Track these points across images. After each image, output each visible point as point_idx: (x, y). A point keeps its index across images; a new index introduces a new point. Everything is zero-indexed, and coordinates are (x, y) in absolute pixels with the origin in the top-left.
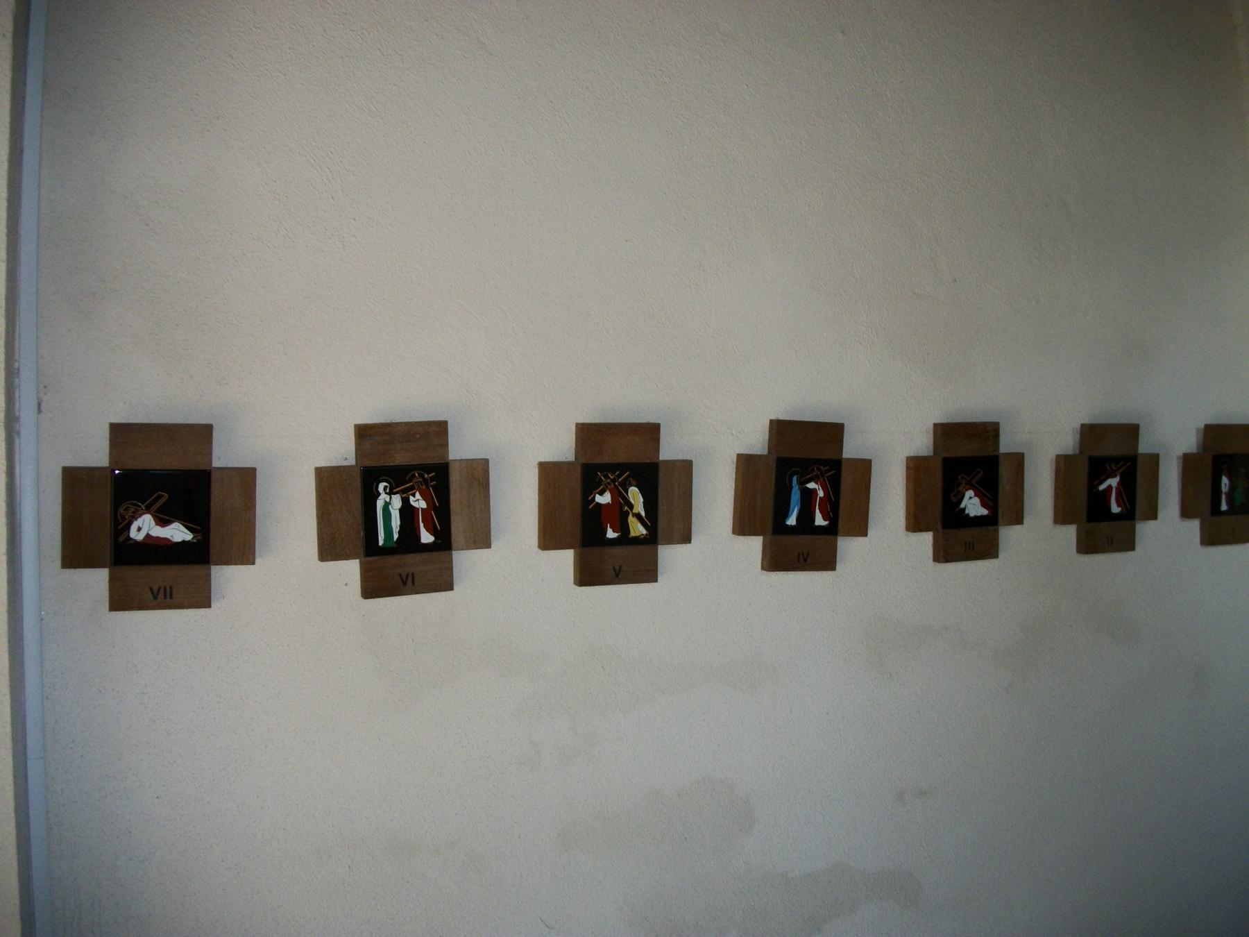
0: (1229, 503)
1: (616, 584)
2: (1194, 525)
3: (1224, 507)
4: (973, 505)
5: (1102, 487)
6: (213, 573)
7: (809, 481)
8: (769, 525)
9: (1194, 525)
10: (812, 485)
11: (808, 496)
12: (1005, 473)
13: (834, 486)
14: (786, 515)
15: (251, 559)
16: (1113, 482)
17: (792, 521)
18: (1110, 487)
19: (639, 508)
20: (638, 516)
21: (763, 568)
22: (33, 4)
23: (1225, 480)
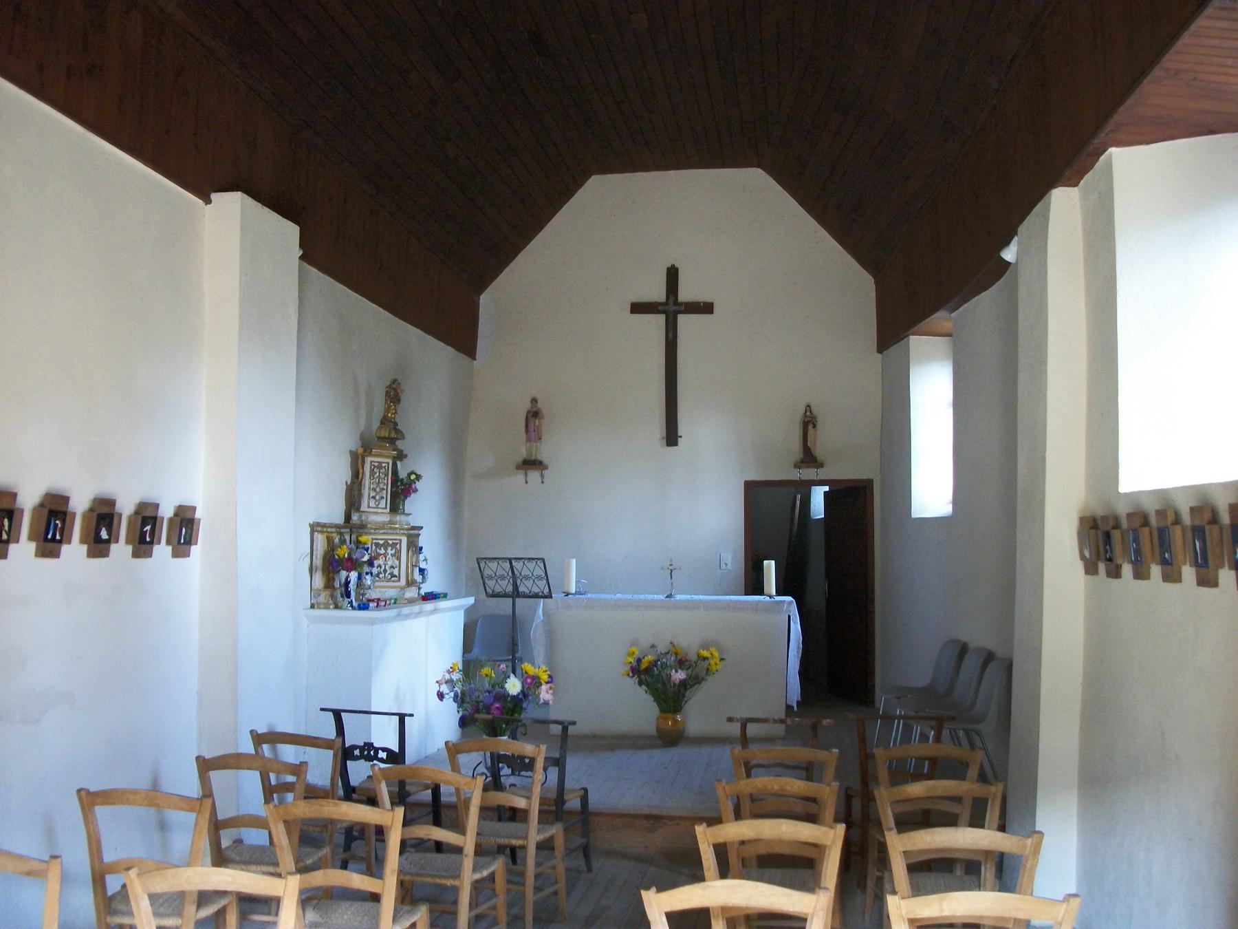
0: (185, 539)
1: (1039, 707)
2: (85, 547)
3: (182, 541)
4: (104, 534)
5: (145, 530)
6: (62, 548)
7: (58, 519)
8: (42, 539)
9: (85, 547)
10: (57, 522)
11: (56, 525)
12: (115, 522)
13: (64, 521)
14: (48, 534)
15: (162, 910)
16: (148, 528)
17: (50, 537)
18: (147, 530)
19: (6, 528)
20: (6, 531)
21: (36, 556)
22: (6, 847)
23: (184, 530)
